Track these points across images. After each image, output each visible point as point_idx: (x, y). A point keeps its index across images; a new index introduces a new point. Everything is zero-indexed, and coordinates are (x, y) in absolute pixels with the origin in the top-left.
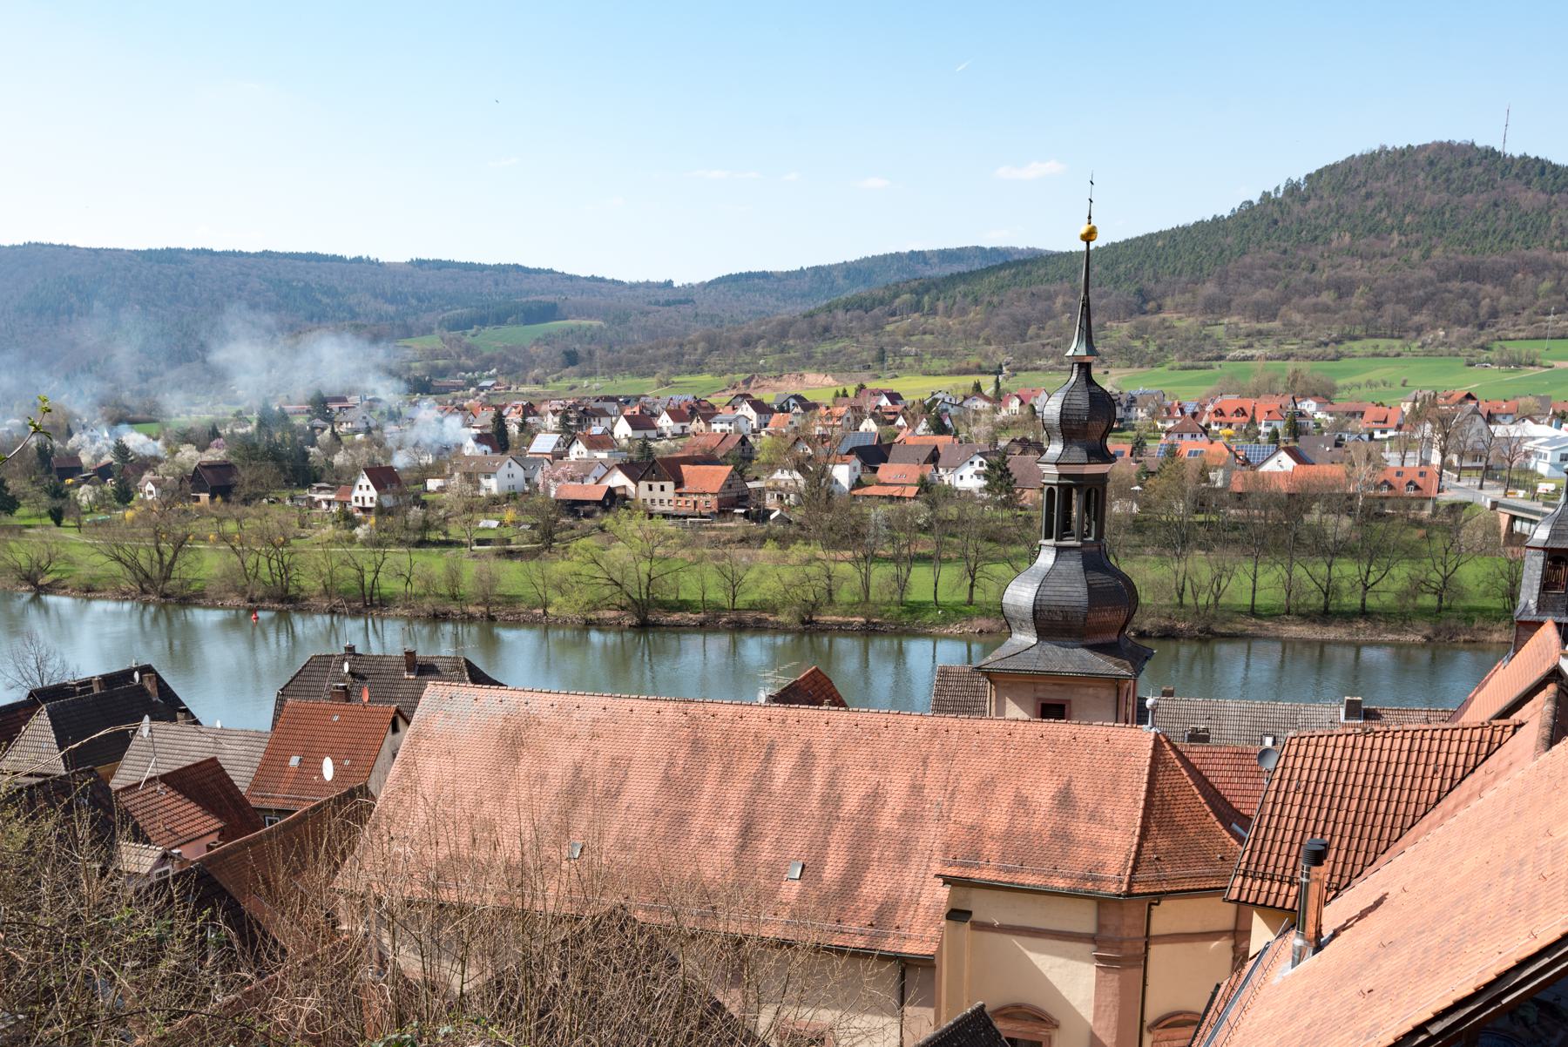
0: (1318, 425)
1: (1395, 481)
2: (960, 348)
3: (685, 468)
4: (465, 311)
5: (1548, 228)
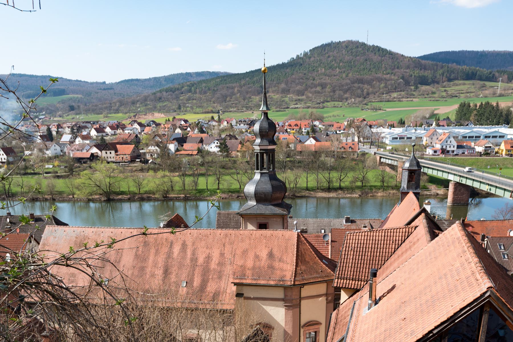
1: (346, 146)
2: (205, 105)
4: (32, 92)
5: (381, 68)
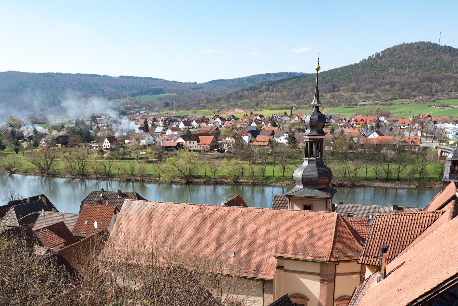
0: (385, 124)
1: (408, 140)
2: (280, 102)
3: (200, 137)
4: (136, 91)
5: (452, 67)
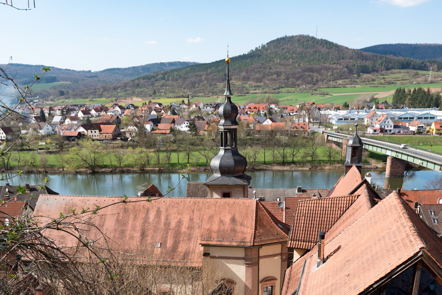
1: (298, 126)
2: (177, 90)
4: (27, 79)
5: (329, 58)
